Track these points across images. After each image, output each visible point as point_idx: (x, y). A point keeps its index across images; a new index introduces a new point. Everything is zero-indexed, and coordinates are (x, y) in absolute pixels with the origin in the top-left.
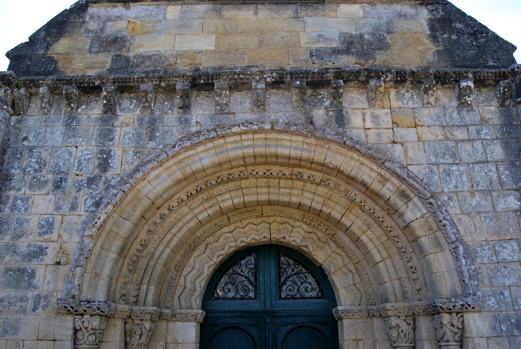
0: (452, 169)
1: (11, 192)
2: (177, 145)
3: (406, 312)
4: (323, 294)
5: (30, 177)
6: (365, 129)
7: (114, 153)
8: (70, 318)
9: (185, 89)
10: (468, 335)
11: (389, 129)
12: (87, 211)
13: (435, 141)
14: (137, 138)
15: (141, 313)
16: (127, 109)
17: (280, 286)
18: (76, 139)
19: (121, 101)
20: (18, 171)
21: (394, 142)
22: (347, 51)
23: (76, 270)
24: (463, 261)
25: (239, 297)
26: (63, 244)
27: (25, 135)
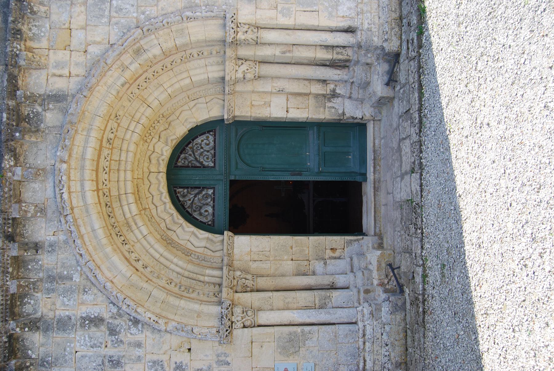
0: (115, 5)
2: (79, 252)
3: (233, 65)
6: (70, 76)
7: (84, 313)
8: (235, 332)
9: (19, 246)
10: (254, 22)
11: (71, 55)
12: (142, 331)
13: (86, 15)
14: (69, 293)
15: (229, 279)
16: (34, 307)
17: (204, 167)
18: (67, 353)
19: (25, 314)
23: (196, 333)
24: (198, 14)
25: (212, 202)
26: (173, 348)
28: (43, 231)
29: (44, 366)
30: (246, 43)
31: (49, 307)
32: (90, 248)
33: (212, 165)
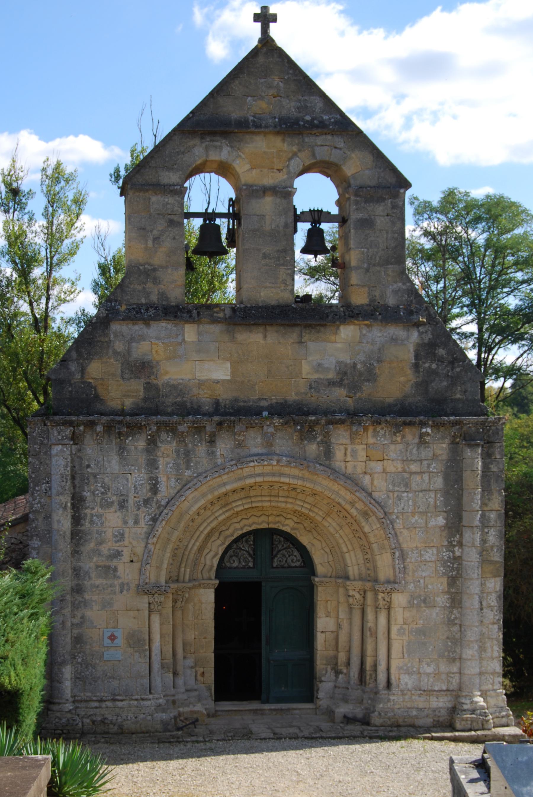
1: (87, 511)
4: (304, 564)
5: (100, 498)
8: (146, 596)
13: (395, 473)
17: (273, 559)
20: (89, 494)
21: (365, 473)
22: (339, 383)
24: (397, 562)
27: (87, 463)
28: (223, 446)
29: (120, 449)
30: (376, 599)
31: (165, 452)
32: (211, 483)
33: (275, 565)
